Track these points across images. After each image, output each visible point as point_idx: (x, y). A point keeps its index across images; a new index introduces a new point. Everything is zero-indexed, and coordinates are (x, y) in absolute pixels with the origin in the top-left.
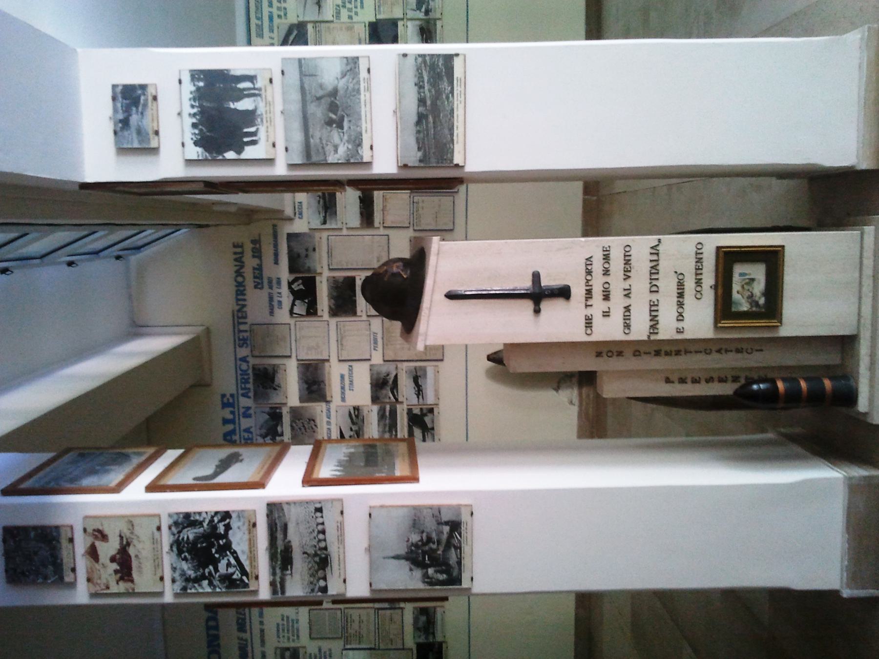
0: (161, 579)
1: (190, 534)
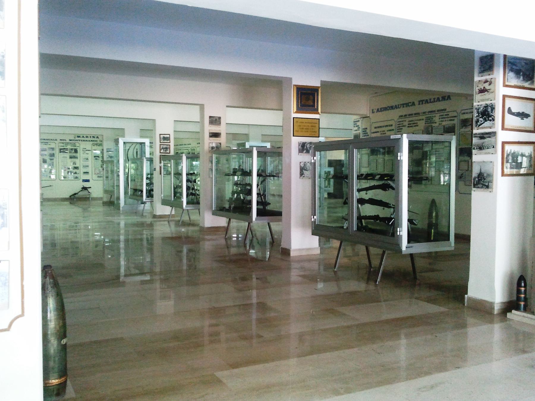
0: (479, 101)
1: (489, 110)
